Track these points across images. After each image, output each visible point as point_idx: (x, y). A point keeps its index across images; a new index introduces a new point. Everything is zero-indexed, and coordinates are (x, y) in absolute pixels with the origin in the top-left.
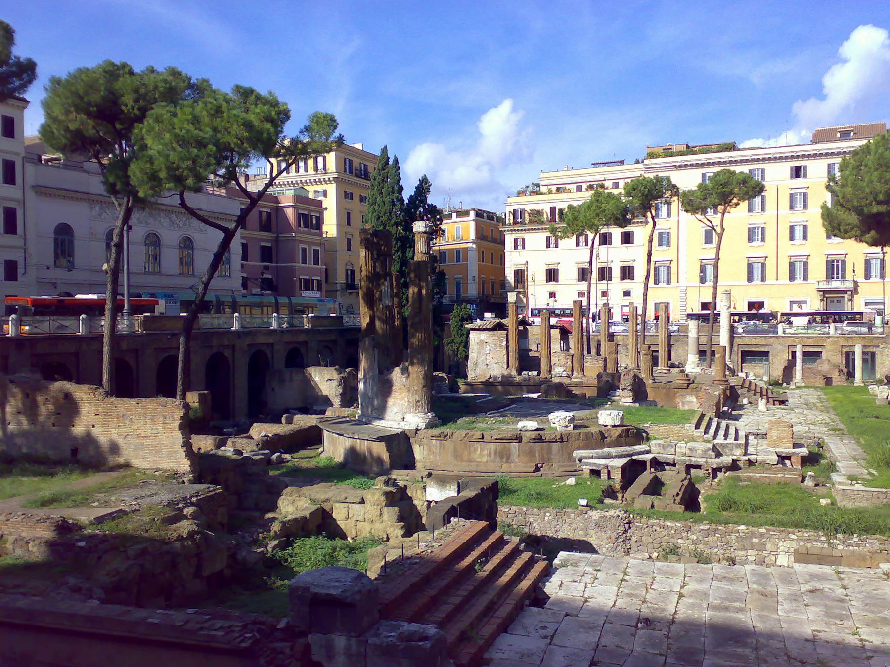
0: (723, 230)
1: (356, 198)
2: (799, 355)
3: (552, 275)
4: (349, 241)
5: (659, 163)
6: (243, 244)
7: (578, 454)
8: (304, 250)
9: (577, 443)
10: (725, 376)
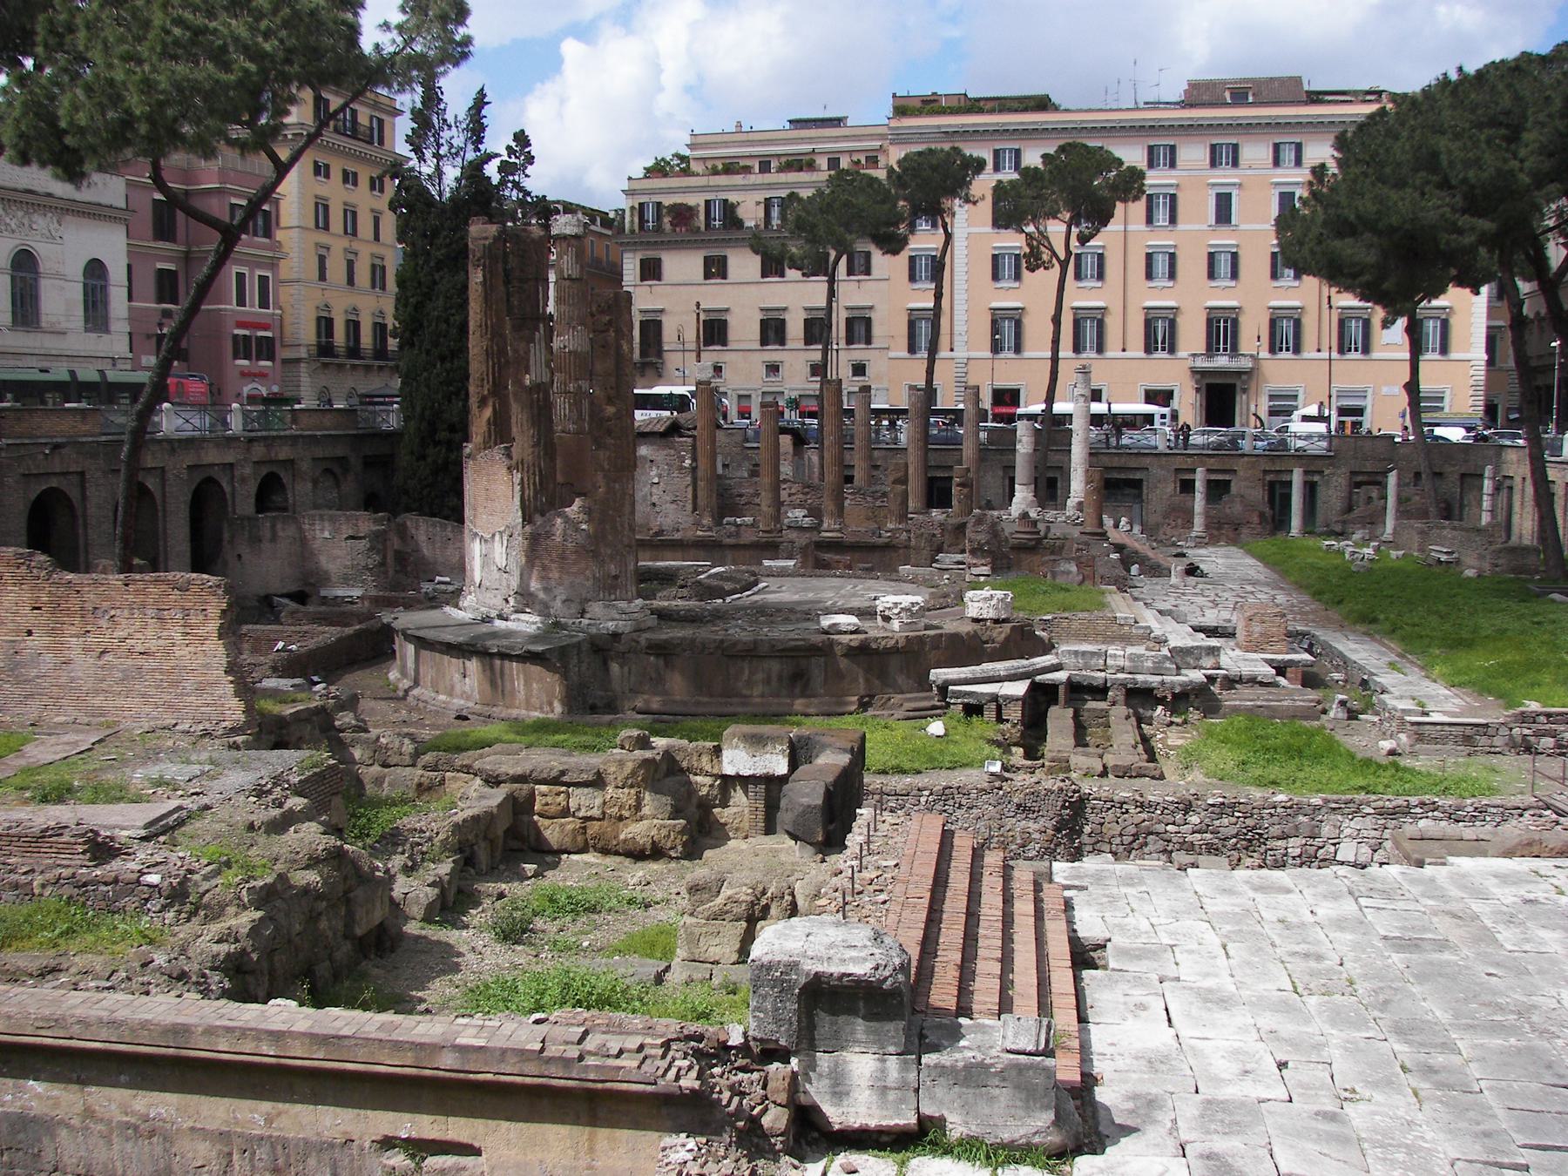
1: (336, 174)
4: (322, 259)
5: (927, 127)
7: (939, 674)
8: (241, 277)
9: (933, 656)
10: (1101, 524)
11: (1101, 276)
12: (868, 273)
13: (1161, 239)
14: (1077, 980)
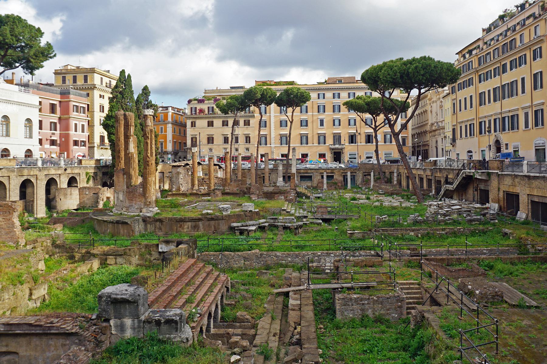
0: (292, 120)
2: (325, 177)
3: (210, 140)
6: (40, 121)
8: (76, 125)
11: (307, 126)
13: (304, 117)
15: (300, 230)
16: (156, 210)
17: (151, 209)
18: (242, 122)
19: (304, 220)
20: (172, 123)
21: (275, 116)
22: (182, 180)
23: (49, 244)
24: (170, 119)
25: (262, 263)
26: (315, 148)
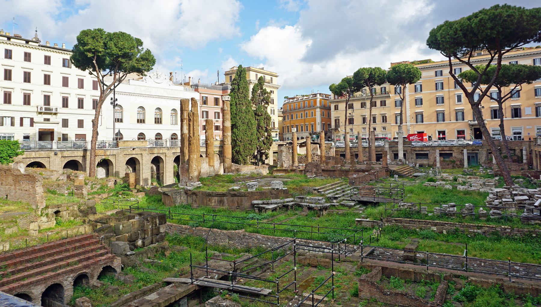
11: (443, 102)
12: (385, 105)
14: (184, 296)
15: (325, 213)
16: (197, 184)
17: (192, 183)
18: (378, 103)
19: (335, 201)
20: (320, 108)
21: (410, 95)
22: (285, 158)
23: (75, 209)
24: (318, 104)
25: (245, 244)
26: (453, 124)
